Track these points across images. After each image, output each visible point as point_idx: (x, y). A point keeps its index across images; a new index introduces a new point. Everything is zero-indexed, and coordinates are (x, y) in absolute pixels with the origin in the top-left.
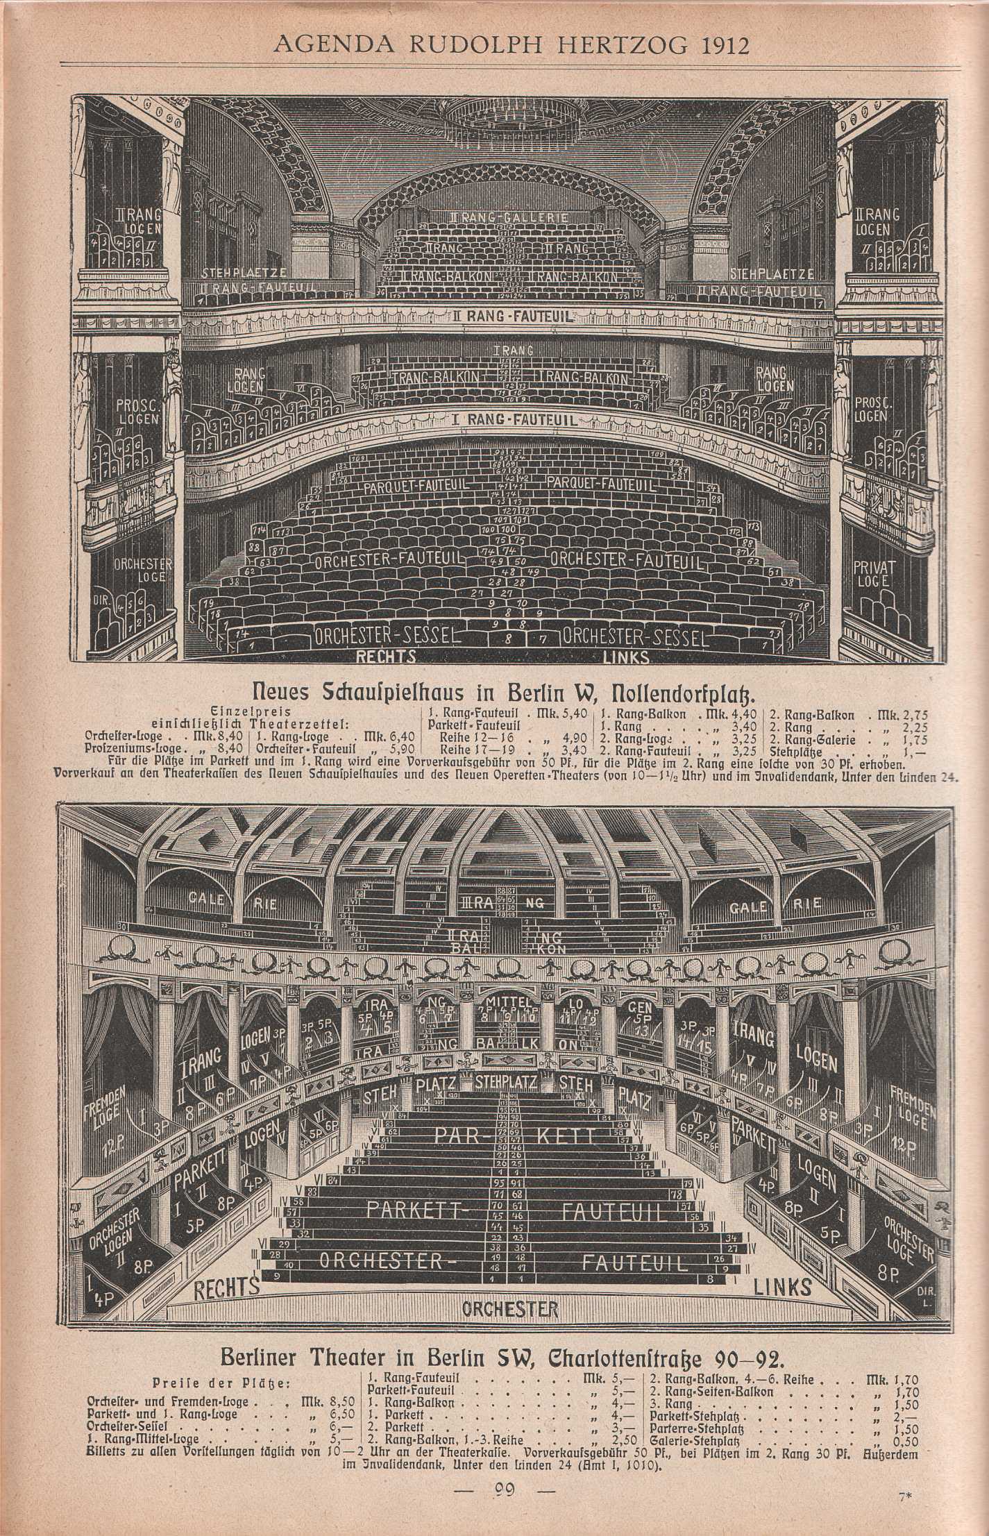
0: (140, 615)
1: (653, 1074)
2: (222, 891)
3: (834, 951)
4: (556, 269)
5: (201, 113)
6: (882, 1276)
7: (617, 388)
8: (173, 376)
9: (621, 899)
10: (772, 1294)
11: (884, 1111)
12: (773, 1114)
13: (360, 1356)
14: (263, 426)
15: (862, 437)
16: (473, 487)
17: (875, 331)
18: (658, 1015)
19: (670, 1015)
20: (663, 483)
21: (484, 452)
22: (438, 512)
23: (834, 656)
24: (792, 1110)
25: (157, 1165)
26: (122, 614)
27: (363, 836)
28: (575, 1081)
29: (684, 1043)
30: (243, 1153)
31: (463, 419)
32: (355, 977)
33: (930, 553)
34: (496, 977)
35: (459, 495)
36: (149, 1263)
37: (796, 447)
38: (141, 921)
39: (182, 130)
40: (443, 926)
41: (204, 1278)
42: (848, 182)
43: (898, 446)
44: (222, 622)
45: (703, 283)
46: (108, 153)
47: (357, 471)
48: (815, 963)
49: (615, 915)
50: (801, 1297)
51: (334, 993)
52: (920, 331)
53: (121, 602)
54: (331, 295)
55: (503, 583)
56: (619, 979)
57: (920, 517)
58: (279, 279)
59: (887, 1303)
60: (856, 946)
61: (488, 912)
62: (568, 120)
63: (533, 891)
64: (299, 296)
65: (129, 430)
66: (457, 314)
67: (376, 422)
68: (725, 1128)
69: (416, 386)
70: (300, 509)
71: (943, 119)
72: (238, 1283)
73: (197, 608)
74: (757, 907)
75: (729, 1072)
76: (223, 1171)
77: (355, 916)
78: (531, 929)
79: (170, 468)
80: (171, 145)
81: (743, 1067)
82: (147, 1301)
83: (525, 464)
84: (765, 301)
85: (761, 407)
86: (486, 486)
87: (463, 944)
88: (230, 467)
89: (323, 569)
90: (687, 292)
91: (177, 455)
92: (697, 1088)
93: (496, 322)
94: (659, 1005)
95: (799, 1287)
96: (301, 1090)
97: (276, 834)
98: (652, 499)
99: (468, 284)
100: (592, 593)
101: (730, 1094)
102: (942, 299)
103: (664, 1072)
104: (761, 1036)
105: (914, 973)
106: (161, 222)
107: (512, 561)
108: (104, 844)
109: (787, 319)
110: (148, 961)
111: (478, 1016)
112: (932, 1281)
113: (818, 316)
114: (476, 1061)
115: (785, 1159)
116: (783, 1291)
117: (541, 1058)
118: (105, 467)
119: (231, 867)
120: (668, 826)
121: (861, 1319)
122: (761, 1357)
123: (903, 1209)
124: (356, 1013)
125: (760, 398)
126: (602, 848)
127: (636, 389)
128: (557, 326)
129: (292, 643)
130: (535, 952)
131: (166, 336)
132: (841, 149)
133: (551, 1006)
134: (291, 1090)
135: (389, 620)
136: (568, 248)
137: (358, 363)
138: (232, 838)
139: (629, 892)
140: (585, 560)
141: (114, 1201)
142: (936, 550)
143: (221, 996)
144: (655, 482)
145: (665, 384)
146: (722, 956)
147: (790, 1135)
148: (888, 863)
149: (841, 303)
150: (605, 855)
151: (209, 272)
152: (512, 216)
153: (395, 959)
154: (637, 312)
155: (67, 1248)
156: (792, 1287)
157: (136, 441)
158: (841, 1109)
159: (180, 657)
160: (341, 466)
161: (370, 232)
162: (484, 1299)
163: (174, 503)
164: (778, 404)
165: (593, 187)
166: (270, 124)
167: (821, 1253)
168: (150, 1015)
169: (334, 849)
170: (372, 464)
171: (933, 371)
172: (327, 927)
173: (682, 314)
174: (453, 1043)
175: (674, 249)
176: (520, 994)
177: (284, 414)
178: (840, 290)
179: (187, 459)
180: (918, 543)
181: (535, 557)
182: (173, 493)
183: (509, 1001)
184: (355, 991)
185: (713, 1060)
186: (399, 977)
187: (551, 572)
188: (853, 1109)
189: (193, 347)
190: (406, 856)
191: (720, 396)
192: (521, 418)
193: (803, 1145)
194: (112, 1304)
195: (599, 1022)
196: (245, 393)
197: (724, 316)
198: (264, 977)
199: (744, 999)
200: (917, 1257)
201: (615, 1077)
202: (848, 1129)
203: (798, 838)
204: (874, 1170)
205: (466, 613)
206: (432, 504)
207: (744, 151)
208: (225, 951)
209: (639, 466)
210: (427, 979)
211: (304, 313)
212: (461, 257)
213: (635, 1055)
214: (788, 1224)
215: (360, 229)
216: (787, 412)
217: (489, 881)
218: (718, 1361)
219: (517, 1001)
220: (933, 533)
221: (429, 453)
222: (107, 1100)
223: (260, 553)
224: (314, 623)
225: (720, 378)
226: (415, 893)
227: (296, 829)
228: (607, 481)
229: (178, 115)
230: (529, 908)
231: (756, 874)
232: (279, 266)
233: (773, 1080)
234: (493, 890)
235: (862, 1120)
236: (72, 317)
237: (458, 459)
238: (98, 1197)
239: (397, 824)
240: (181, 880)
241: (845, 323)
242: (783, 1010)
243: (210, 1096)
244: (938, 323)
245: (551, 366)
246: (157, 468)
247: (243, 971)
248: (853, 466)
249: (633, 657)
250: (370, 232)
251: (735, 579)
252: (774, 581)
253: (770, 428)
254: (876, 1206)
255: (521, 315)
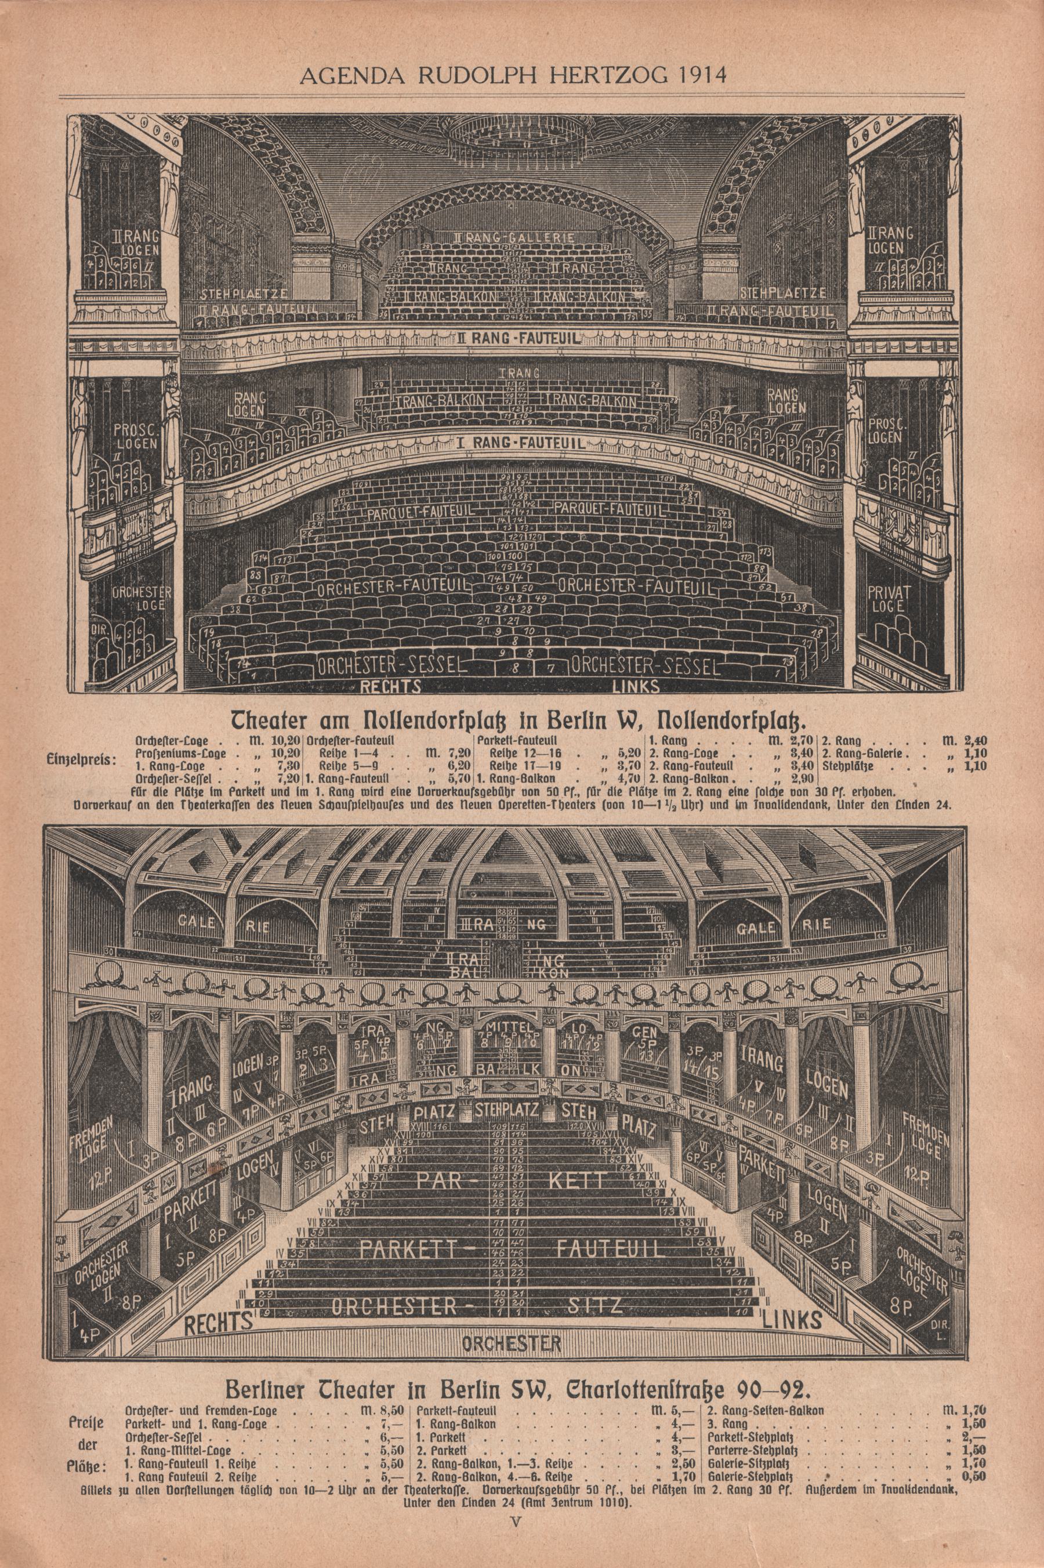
0: (139, 645)
1: (658, 1100)
2: (212, 914)
3: (845, 974)
4: (564, 289)
5: (197, 131)
6: (895, 1309)
7: (625, 410)
8: (171, 400)
9: (625, 919)
10: (781, 1327)
11: (897, 1141)
12: (781, 1142)
13: (368, 1389)
14: (264, 451)
15: (877, 459)
16: (478, 513)
17: (888, 352)
18: (663, 1040)
19: (675, 1037)
20: (673, 508)
21: (491, 477)
22: (443, 539)
23: (848, 685)
24: (801, 1138)
25: (147, 1198)
26: (120, 643)
27: (357, 858)
28: (578, 1108)
29: (690, 1069)
30: (234, 1185)
31: (468, 441)
32: (351, 1003)
33: (946, 578)
34: (496, 1002)
35: (464, 521)
36: (137, 1299)
37: (808, 469)
38: (129, 945)
39: (180, 149)
40: (442, 949)
41: (194, 1312)
42: (860, 200)
43: (913, 468)
44: (223, 652)
45: (713, 302)
46: (105, 174)
47: (361, 498)
48: (824, 986)
49: (619, 937)
50: (810, 1330)
51: (328, 1019)
52: (934, 351)
53: (120, 631)
54: (332, 317)
55: (509, 610)
56: (624, 1004)
57: (935, 541)
58: (279, 301)
59: (900, 1336)
60: (870, 969)
61: (489, 935)
62: (575, 138)
63: (535, 912)
64: (301, 318)
65: (128, 455)
66: (461, 336)
67: (380, 446)
68: (732, 1158)
69: (421, 410)
70: (302, 537)
71: (957, 134)
72: (230, 1319)
73: (197, 637)
74: (765, 928)
75: (737, 1098)
76: (216, 1200)
77: (352, 939)
78: (533, 952)
79: (169, 495)
80: (168, 166)
81: (752, 1095)
82: (135, 1336)
83: (532, 489)
84: (776, 321)
85: (772, 428)
86: (493, 512)
87: (462, 968)
88: (230, 494)
89: (325, 597)
90: (696, 311)
91: (176, 482)
92: (703, 1115)
93: (501, 343)
94: (665, 1030)
95: (809, 1320)
96: (295, 1120)
97: (267, 856)
98: (661, 524)
99: (473, 305)
100: (602, 620)
101: (738, 1122)
102: (957, 318)
103: (669, 1098)
104: (770, 1061)
105: (926, 997)
106: (159, 243)
107: (519, 589)
108: (96, 869)
109: (799, 340)
110: (135, 988)
111: (477, 1040)
112: (946, 1314)
113: (831, 337)
114: (476, 1089)
115: (795, 1188)
116: (792, 1324)
117: (543, 1085)
118: (103, 494)
119: (222, 890)
120: (673, 845)
121: (872, 1352)
122: (785, 1388)
123: (916, 1239)
124: (352, 1038)
125: (771, 420)
126: (606, 868)
127: (644, 412)
128: (563, 348)
129: (296, 673)
130: (536, 976)
131: (164, 360)
132: (853, 166)
133: (553, 1031)
134: (285, 1120)
135: (394, 649)
136: (575, 268)
137: (360, 386)
138: (222, 860)
139: (633, 914)
140: (593, 587)
141: (101, 1235)
142: (952, 574)
143: (212, 1023)
144: (664, 507)
145: (674, 406)
146: (729, 980)
147: (799, 1164)
148: (899, 884)
149: (854, 323)
150: (610, 879)
151: (208, 293)
152: (517, 236)
153: (392, 985)
154: (645, 334)
155: (51, 1281)
156: (802, 1320)
157: (135, 465)
158: (852, 1139)
159: (181, 688)
160: (343, 493)
161: (372, 252)
162: (485, 1334)
163: (173, 531)
164: (790, 426)
165: (600, 206)
166: (270, 142)
167: (831, 1284)
168: (139, 1040)
169: (327, 872)
170: (376, 490)
171: (949, 392)
172: (322, 951)
173: (691, 335)
174: (452, 1069)
175: (685, 268)
176: (518, 1019)
177: (285, 438)
178: (853, 309)
179: (187, 486)
180: (934, 568)
181: (542, 582)
182: (172, 521)
183: (510, 1026)
184: (352, 1017)
185: (721, 1084)
186: (396, 1002)
187: (558, 599)
188: (864, 1138)
189: (194, 371)
190: (403, 879)
191: (732, 418)
192: (527, 441)
193: (813, 1175)
194: (98, 1340)
195: (603, 1048)
196: (245, 417)
197: (734, 337)
198: (258, 1004)
199: (752, 1024)
200: (931, 1290)
201: (618, 1104)
202: (861, 1158)
203: (807, 858)
204: (887, 1198)
205: (472, 642)
206: (436, 530)
207: (754, 168)
208: (216, 977)
209: (648, 491)
210: (424, 1005)
211: (305, 335)
212: (465, 277)
213: (638, 1081)
214: (798, 1255)
215: (361, 249)
216: (798, 434)
217: (490, 903)
218: (740, 1391)
219: (518, 1027)
220: (949, 557)
221: (434, 479)
222: (93, 1131)
223: (262, 581)
224: (317, 652)
225: (734, 401)
226: (414, 915)
227: (290, 850)
228: (616, 507)
229: (176, 133)
230: (531, 930)
231: (763, 894)
232: (280, 287)
233: (782, 1107)
234: (494, 911)
235: (873, 1147)
236: (69, 340)
237: (464, 484)
238: (85, 1229)
239: (391, 845)
240: (167, 903)
241: (858, 344)
242: (792, 1033)
243: (201, 1126)
244: (953, 343)
245: (558, 389)
246: (155, 495)
247: (235, 997)
248: (864, 489)
249: (643, 686)
250: (372, 252)
251: (747, 605)
252: (787, 607)
253: (782, 450)
254: (892, 1238)
255: (526, 337)
